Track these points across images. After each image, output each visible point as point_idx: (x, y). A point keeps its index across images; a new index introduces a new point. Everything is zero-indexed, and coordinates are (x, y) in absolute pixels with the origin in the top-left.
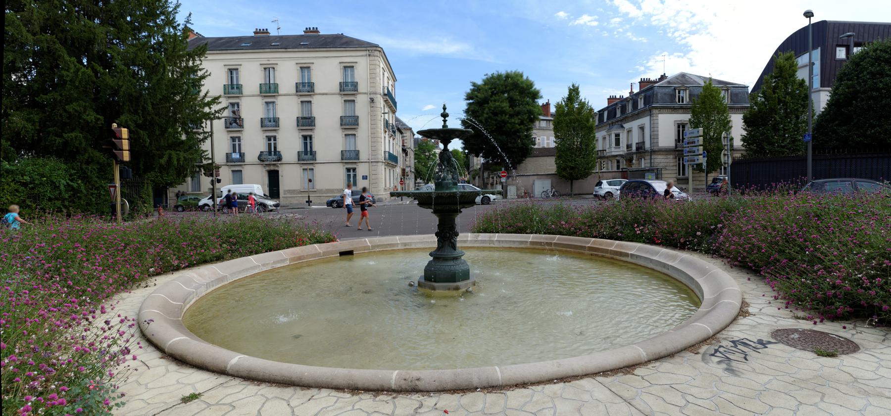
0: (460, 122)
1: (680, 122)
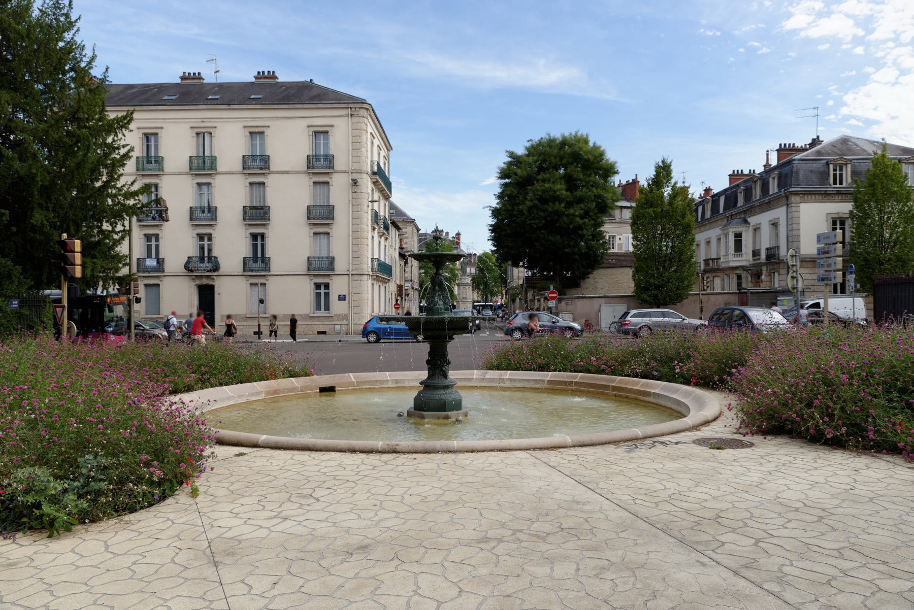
0: (491, 212)
1: (836, 216)
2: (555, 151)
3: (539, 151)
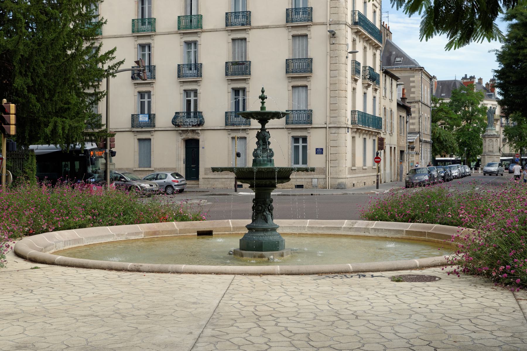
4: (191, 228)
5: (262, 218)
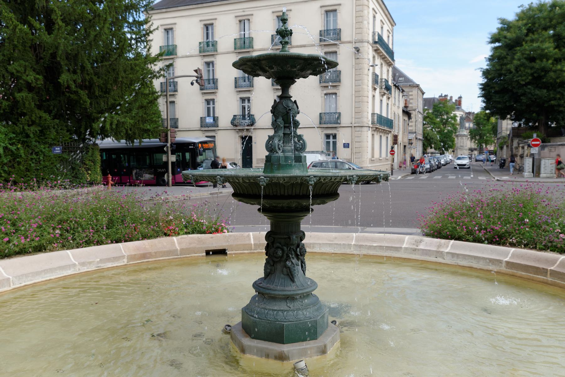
0: (481, 73)
2: (545, 14)
3: (528, 15)
4: (198, 246)
5: (282, 271)
